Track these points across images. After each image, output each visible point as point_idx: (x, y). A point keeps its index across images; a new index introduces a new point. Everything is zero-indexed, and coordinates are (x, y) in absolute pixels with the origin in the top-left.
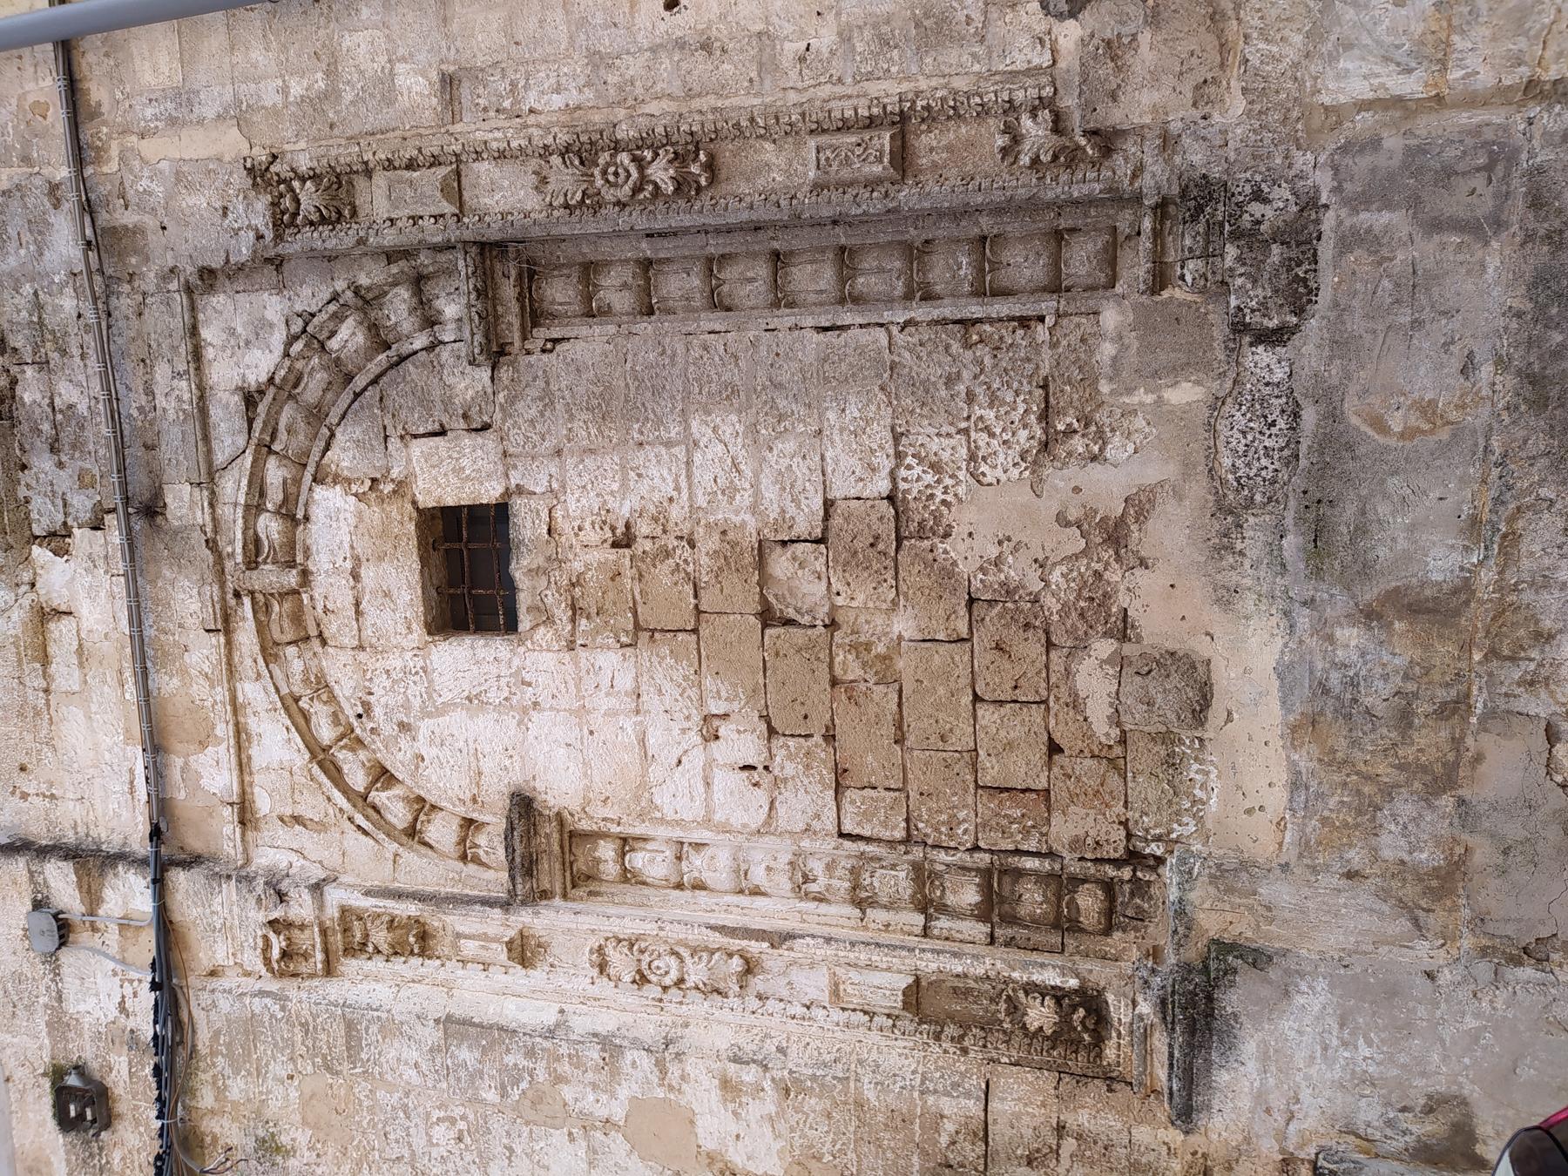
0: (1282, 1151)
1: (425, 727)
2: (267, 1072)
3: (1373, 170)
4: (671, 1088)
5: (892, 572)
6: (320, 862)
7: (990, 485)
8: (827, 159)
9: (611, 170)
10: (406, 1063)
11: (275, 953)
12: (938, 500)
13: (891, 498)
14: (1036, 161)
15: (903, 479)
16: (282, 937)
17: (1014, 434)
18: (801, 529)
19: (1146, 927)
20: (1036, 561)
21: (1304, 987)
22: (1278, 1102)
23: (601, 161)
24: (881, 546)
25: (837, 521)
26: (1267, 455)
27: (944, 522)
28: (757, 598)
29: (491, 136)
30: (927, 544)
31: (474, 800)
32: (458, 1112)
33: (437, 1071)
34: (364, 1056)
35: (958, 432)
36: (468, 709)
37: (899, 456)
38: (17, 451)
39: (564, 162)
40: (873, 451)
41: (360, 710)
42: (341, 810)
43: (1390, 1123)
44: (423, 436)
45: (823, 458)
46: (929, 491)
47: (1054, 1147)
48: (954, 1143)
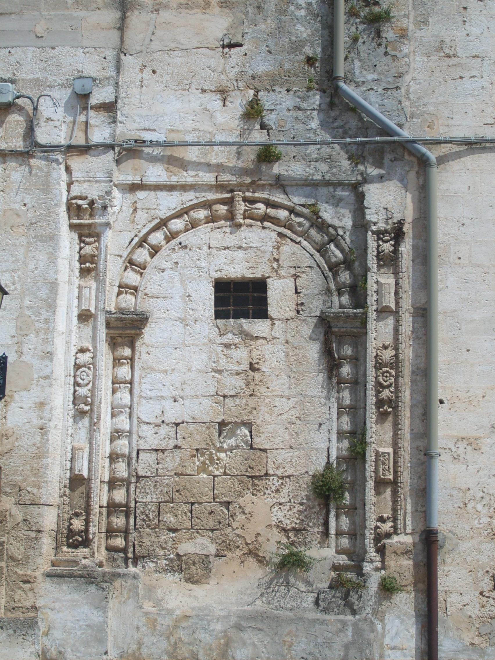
0: (40, 607)
1: (176, 275)
2: (26, 193)
3: (364, 630)
4: (38, 381)
5: (240, 474)
6: (117, 220)
7: (271, 510)
8: (385, 456)
9: (388, 375)
10: (37, 263)
11: (80, 202)
12: (266, 491)
13: (267, 474)
14: (378, 527)
15: (273, 479)
16: (87, 206)
17: (288, 519)
18: (256, 440)
19: (111, 562)
20: (243, 526)
21: (99, 613)
22: (57, 605)
23: (391, 371)
24: (249, 469)
25: (259, 453)
26: (278, 601)
27: (258, 493)
28: (230, 421)
29: (403, 328)
30: (250, 487)
31: (146, 295)
32: (18, 286)
33: (35, 277)
34: (38, 243)
35: (290, 500)
36: (184, 295)
37: (282, 478)
38: (295, 89)
39: (392, 356)
40: (284, 468)
41: (183, 244)
42: (140, 231)
43: (54, 640)
44: (295, 284)
45: (282, 449)
46: (269, 488)
47: (31, 529)
48: (29, 492)
